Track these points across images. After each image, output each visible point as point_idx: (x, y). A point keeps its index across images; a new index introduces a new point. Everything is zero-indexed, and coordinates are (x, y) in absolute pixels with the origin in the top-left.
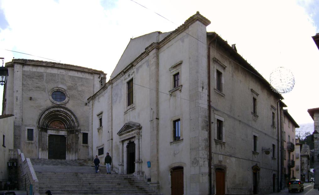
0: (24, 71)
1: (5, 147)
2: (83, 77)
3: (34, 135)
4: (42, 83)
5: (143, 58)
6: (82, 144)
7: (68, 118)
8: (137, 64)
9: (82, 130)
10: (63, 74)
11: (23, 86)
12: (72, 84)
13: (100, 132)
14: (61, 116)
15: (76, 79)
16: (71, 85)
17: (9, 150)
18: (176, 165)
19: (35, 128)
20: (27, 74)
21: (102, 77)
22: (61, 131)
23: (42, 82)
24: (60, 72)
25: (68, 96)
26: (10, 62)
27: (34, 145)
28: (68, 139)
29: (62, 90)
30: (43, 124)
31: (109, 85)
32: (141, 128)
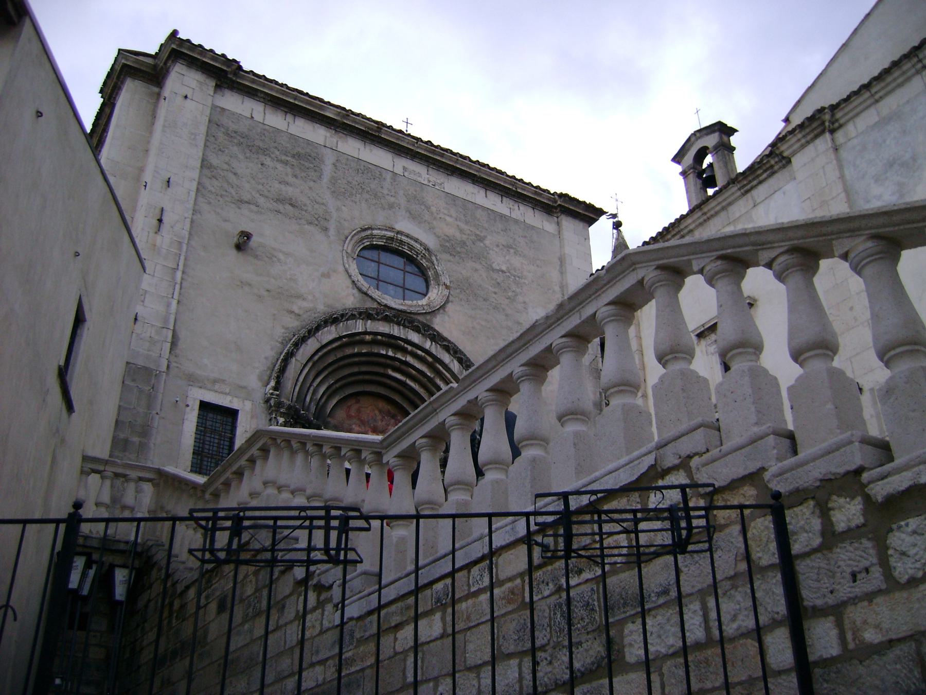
0: (214, 107)
2: (514, 216)
4: (310, 188)
10: (419, 179)
11: (206, 171)
16: (458, 235)
17: (86, 458)
19: (248, 405)
20: (233, 127)
23: (312, 184)
24: (405, 169)
25: (445, 279)
29: (411, 248)
30: (301, 397)
31: (803, 147)
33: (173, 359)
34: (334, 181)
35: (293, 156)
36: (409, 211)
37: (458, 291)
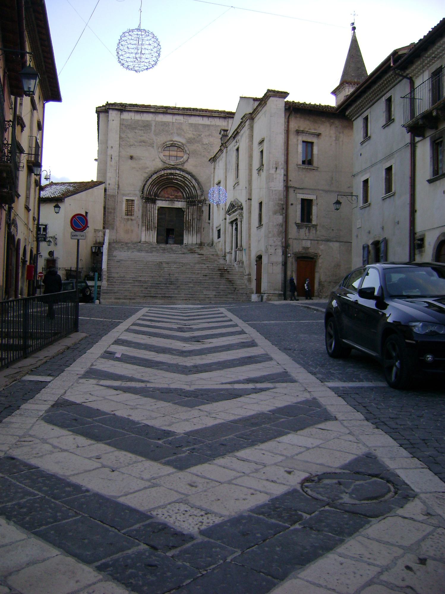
2: (212, 124)
7: (187, 183)
10: (181, 122)
12: (194, 135)
16: (193, 136)
22: (176, 203)
23: (149, 134)
25: (188, 152)
27: (135, 222)
30: (149, 193)
34: (155, 131)
35: (143, 127)
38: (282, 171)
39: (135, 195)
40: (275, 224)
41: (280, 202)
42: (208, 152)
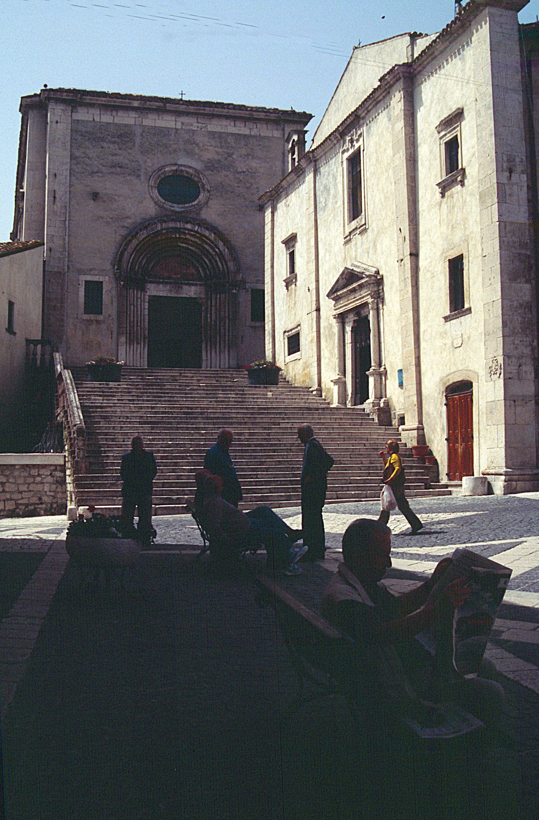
0: (73, 121)
1: (15, 334)
2: (253, 133)
3: (106, 298)
4: (129, 153)
5: (379, 99)
6: (248, 323)
7: (207, 247)
8: (366, 114)
9: (248, 280)
11: (74, 162)
12: (217, 153)
13: (292, 289)
14: (186, 243)
15: (230, 139)
16: (217, 157)
18: (458, 378)
19: (107, 277)
20: (84, 130)
21: (294, 140)
22: (185, 287)
23: (129, 151)
25: (207, 187)
26: (35, 95)
27: (104, 326)
28: (206, 309)
29: (187, 172)
31: (308, 166)
32: (382, 278)
33: (70, 264)
36: (185, 151)
37: (215, 192)
38: (524, 177)
39: (102, 272)
40: (515, 304)
41: (524, 252)
42: (248, 188)
